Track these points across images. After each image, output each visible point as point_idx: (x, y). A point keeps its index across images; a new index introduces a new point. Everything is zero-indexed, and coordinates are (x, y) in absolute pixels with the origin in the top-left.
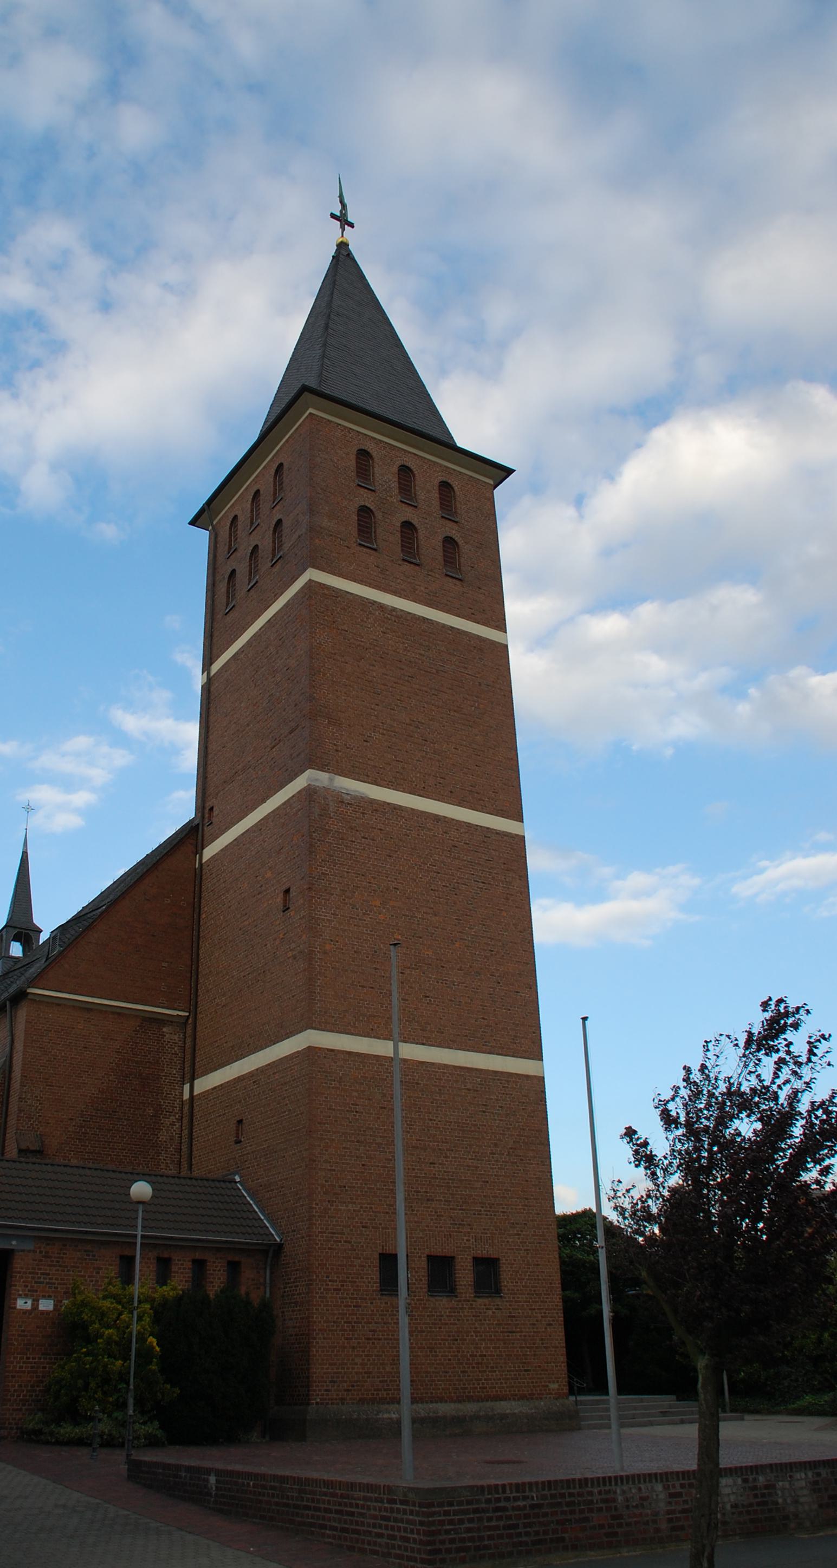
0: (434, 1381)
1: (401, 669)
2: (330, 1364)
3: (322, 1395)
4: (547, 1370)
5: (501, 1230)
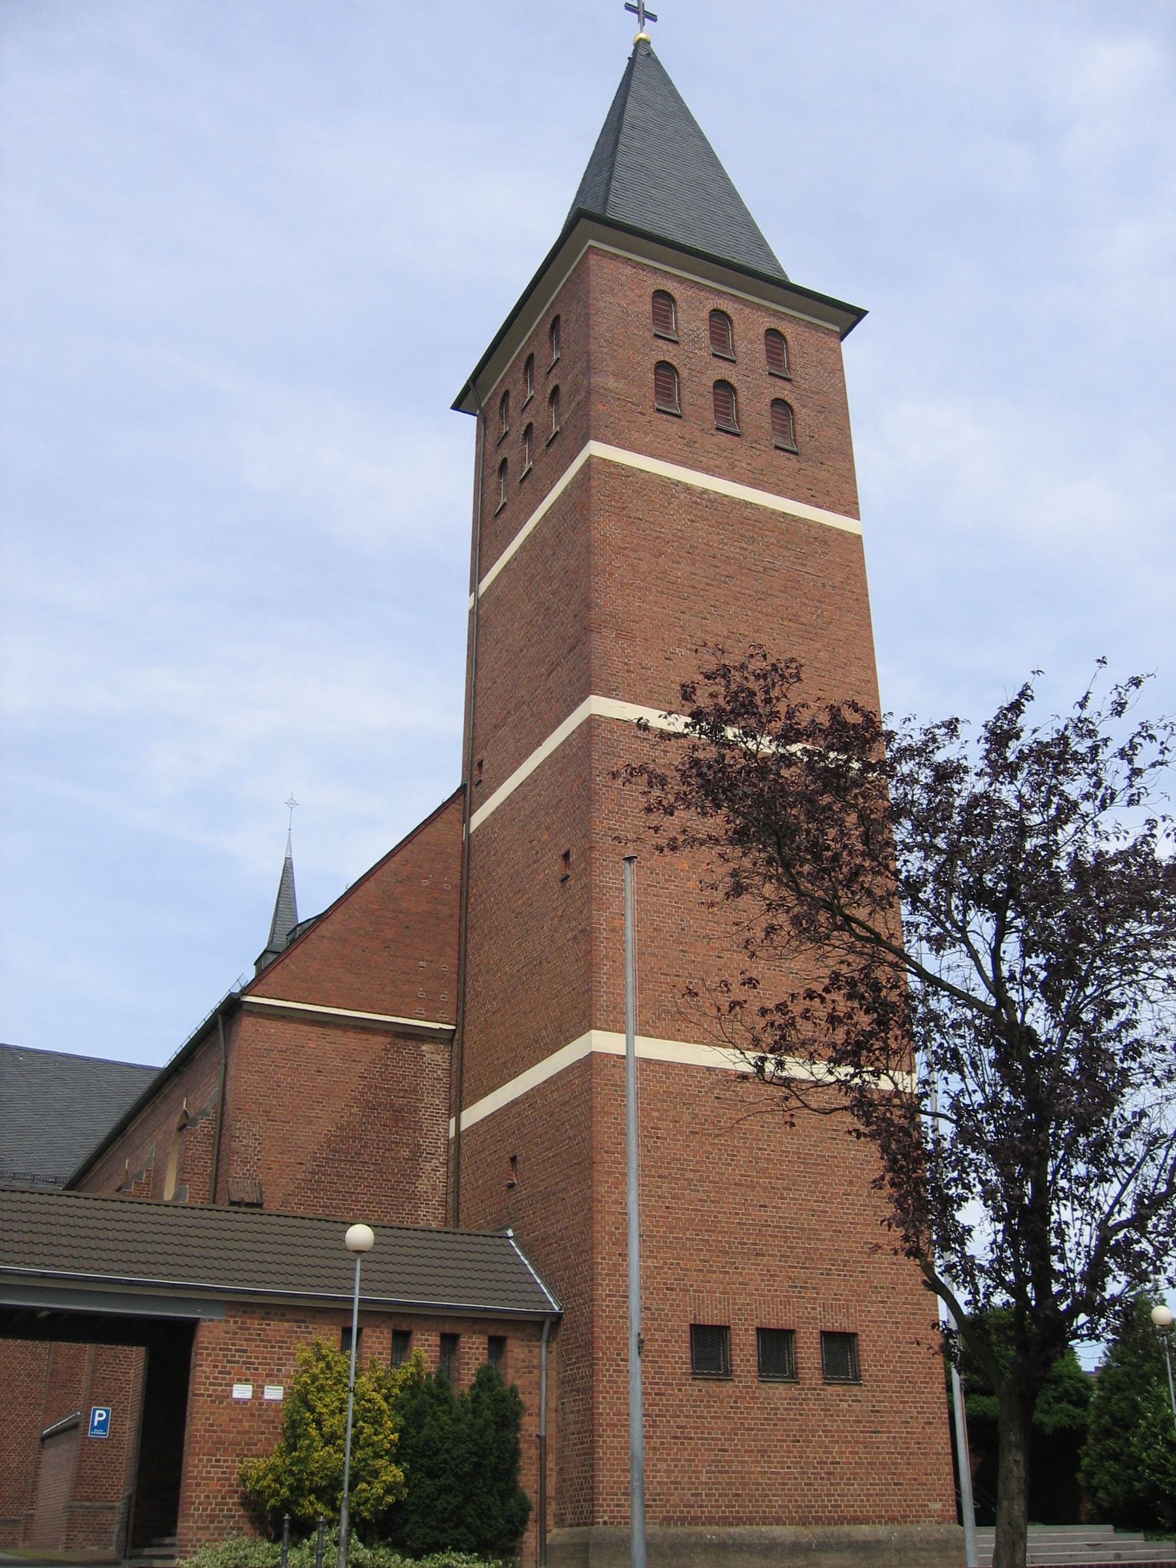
0: (767, 1496)
1: (715, 566)
2: (623, 1471)
3: (612, 1511)
4: (926, 1485)
5: (859, 1295)
